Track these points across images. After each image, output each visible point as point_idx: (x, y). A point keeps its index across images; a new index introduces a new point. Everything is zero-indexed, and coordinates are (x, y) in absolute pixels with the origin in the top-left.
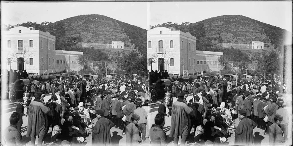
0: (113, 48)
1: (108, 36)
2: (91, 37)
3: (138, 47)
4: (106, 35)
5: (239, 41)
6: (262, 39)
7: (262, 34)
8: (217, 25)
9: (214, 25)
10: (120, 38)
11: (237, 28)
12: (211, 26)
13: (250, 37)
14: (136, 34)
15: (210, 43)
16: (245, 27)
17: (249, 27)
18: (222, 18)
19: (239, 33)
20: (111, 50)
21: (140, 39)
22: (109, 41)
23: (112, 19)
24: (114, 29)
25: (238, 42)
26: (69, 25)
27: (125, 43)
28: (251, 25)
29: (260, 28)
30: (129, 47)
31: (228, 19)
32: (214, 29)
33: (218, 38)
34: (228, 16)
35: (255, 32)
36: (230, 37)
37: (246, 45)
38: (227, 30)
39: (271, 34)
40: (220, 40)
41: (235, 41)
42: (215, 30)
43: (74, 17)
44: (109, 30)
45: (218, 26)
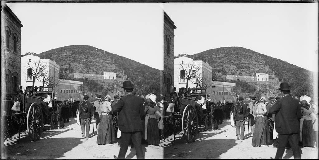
1: (252, 69)
2: (235, 69)
3: (130, 78)
4: (249, 67)
5: (243, 73)
6: (266, 71)
8: (218, 57)
9: (215, 57)
11: (87, 59)
12: (212, 58)
13: (253, 69)
14: (278, 67)
15: (62, 73)
16: (248, 59)
17: (251, 59)
18: (71, 48)
19: (90, 63)
20: (256, 83)
21: (283, 71)
22: (253, 74)
23: (100, 50)
25: (242, 74)
26: (210, 57)
27: (270, 75)
30: (274, 79)
31: (76, 49)
32: (63, 59)
33: (69, 69)
34: (228, 48)
35: (106, 62)
36: (81, 68)
37: (98, 75)
38: (76, 60)
39: (274, 66)
40: (71, 71)
41: (239, 73)
42: (64, 60)
43: (62, 48)
45: (67, 56)
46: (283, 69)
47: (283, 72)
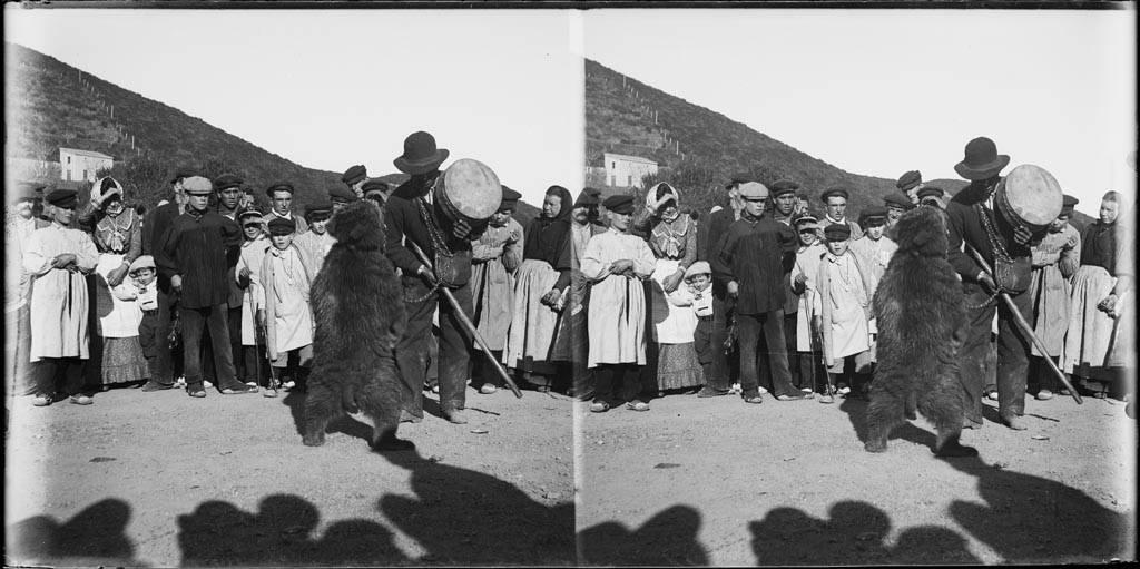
0: (64, 177)
6: (107, 144)
7: (104, 125)
10: (642, 145)
14: (164, 132)
24: (70, 103)
28: (57, 84)
29: (99, 102)
44: (595, 112)
46: (725, 147)
47: (724, 161)
